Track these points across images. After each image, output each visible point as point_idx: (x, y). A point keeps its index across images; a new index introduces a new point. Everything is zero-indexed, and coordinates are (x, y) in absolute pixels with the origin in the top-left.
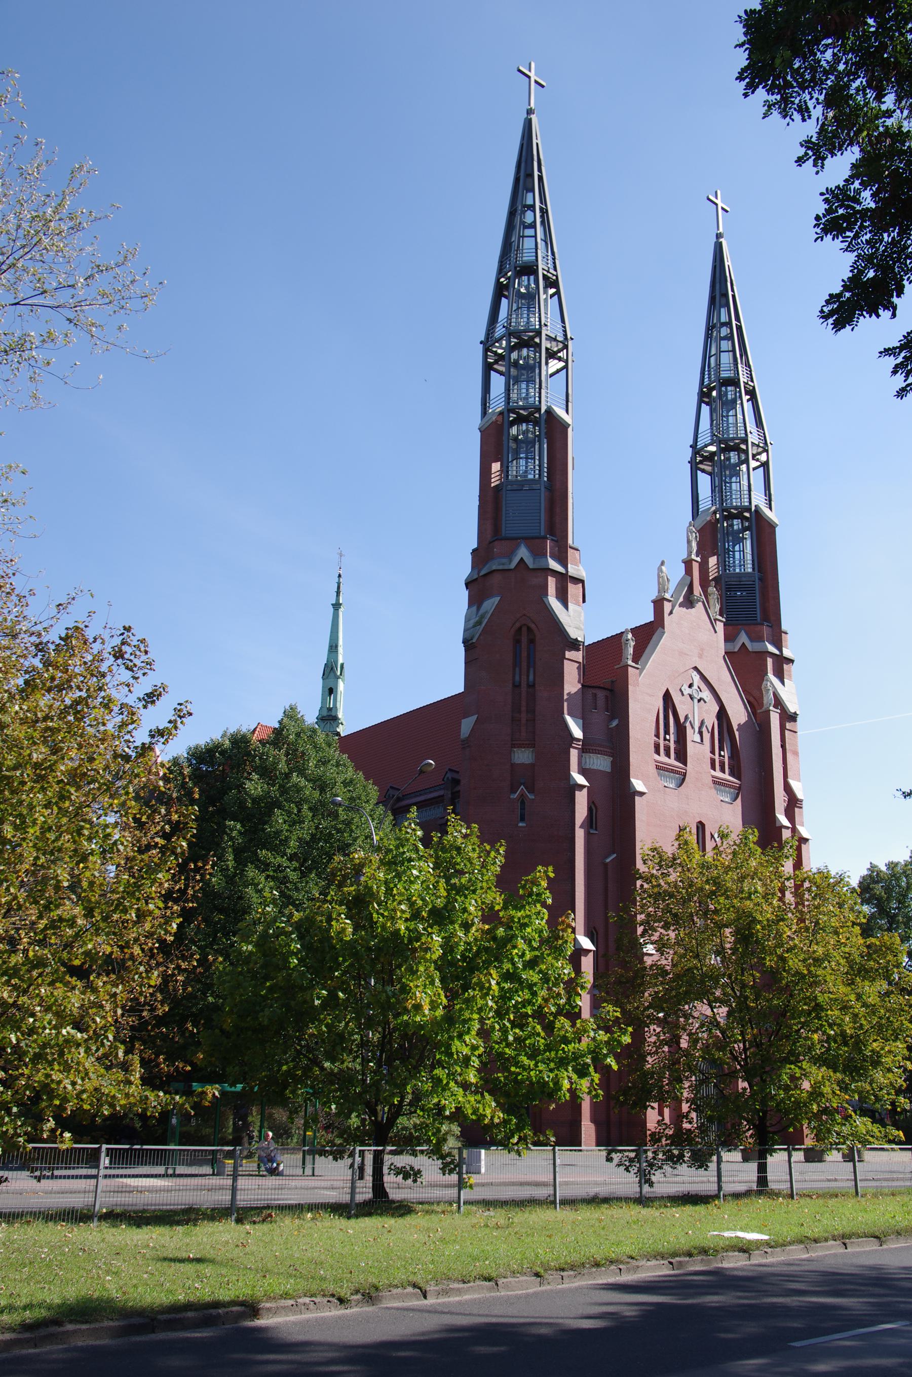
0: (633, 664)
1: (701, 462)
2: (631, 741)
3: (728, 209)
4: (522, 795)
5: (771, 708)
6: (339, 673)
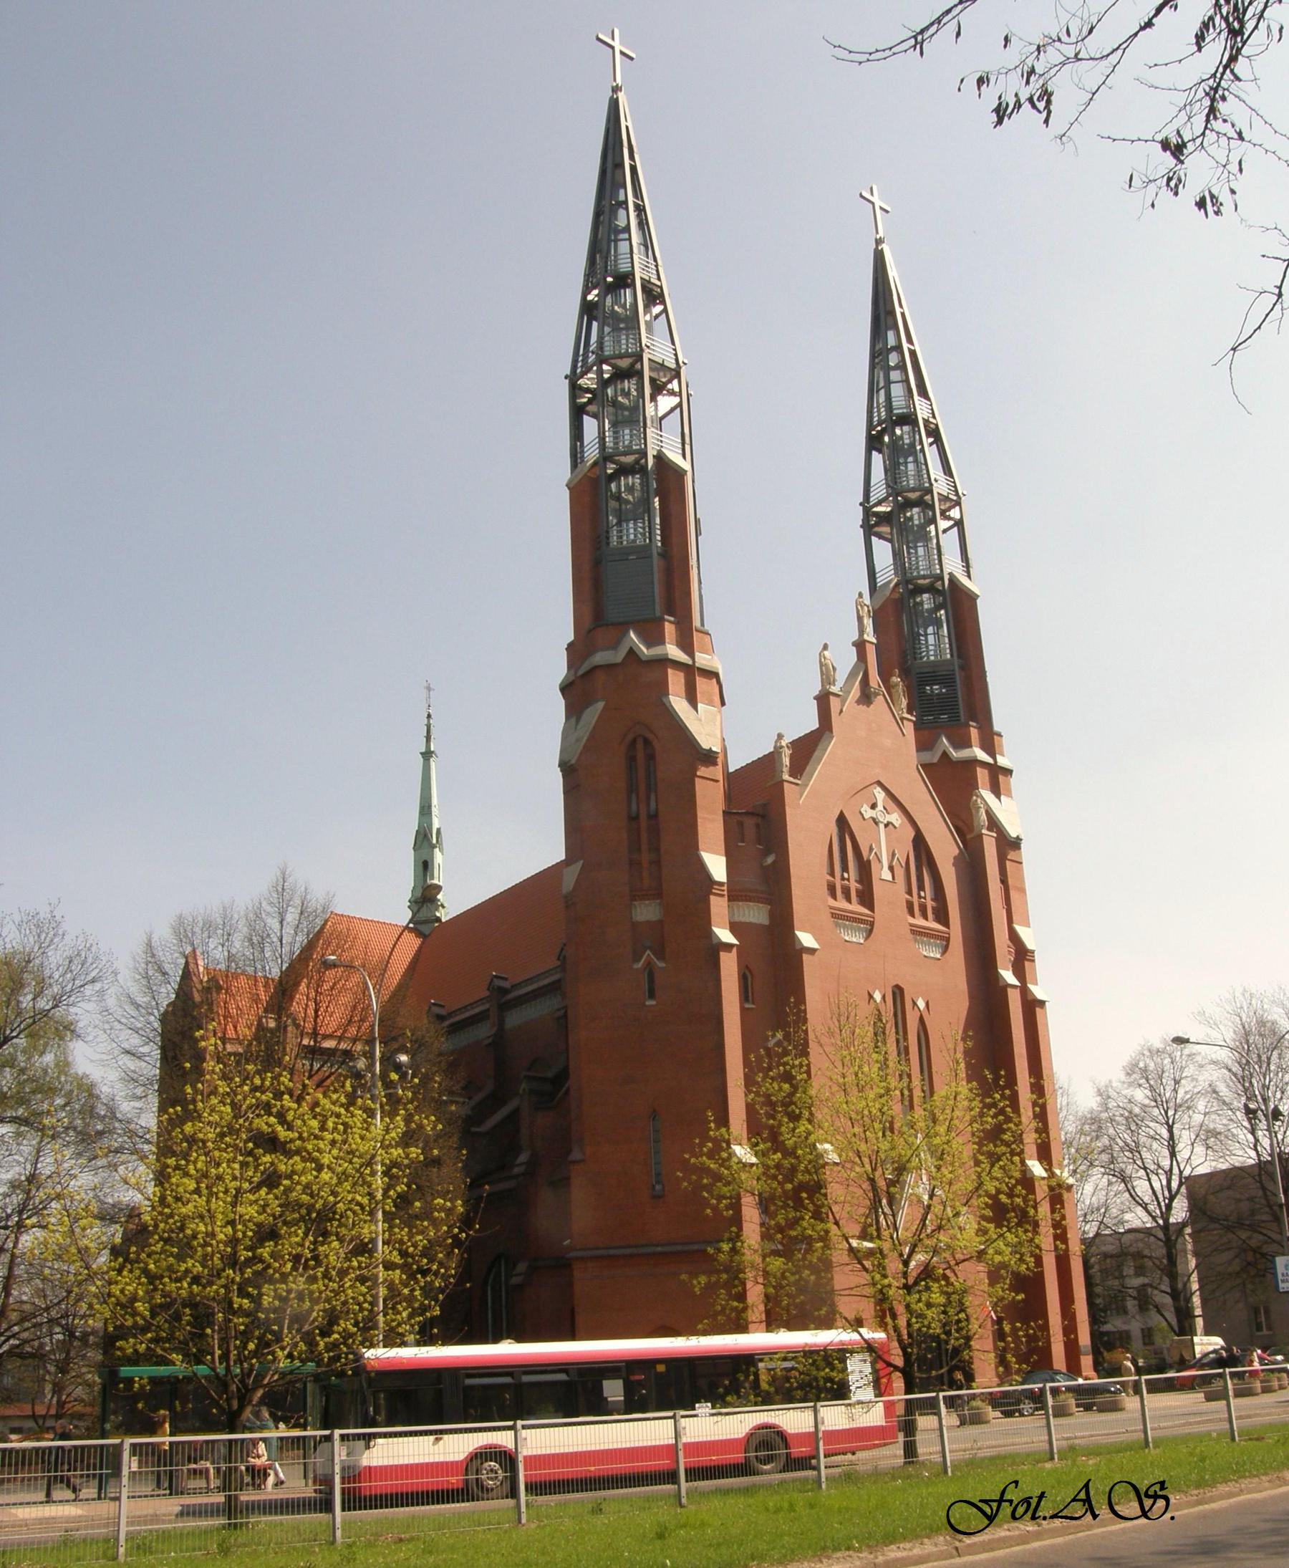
0: (791, 779)
1: (877, 524)
2: (793, 880)
3: (889, 209)
4: (649, 964)
5: (984, 831)
6: (434, 841)
